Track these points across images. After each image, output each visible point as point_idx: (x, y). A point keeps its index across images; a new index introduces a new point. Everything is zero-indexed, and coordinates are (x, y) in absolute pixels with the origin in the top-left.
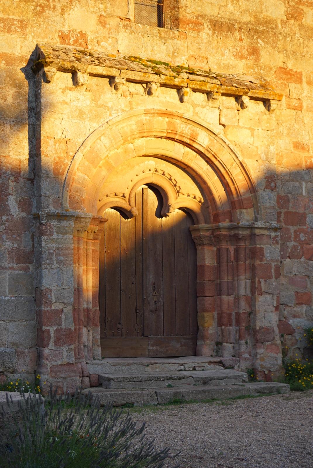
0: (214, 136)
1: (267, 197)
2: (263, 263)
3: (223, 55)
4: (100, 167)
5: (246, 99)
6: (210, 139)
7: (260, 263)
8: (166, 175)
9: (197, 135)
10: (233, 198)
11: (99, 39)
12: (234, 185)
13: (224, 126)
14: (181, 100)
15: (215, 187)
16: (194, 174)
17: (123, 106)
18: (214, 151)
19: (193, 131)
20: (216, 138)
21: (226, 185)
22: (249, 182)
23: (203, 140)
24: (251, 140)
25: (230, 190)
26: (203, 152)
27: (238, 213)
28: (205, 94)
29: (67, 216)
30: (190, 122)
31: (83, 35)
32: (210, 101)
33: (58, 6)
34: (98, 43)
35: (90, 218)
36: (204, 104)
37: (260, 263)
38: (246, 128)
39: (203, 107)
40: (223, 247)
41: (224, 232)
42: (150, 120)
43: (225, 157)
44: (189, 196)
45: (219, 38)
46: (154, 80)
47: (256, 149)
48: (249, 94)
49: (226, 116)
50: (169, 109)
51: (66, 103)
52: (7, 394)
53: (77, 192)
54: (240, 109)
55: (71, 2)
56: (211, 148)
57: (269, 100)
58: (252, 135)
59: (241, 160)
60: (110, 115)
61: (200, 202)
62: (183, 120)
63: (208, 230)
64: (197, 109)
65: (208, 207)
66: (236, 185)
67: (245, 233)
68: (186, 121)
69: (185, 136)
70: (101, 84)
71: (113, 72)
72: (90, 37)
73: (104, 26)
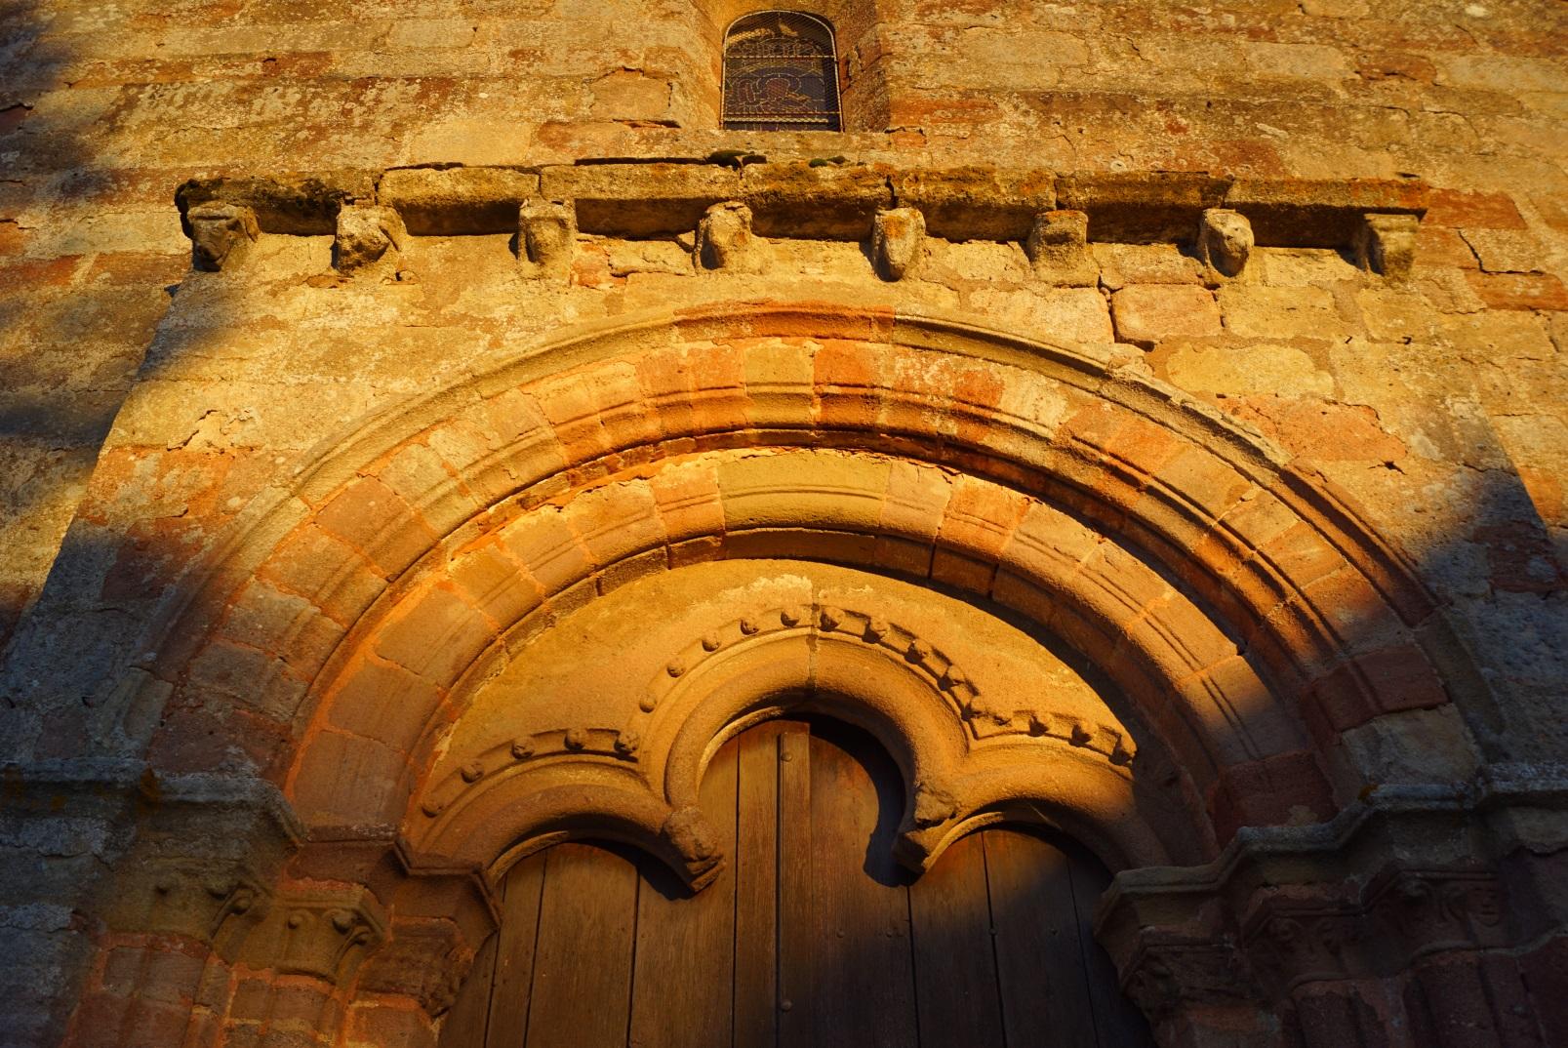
0: (1092, 383)
1: (1529, 635)
6: (1073, 402)
8: (889, 636)
9: (997, 389)
10: (1303, 673)
12: (1280, 593)
13: (1147, 346)
14: (888, 272)
15: (1174, 641)
16: (1042, 607)
18: (1108, 445)
19: (969, 375)
21: (1232, 615)
22: (1370, 565)
23: (1035, 404)
24: (1325, 384)
25: (1237, 594)
26: (1049, 465)
27: (1359, 750)
28: (1015, 245)
29: (66, 787)
30: (941, 341)
32: (1043, 260)
35: (242, 805)
36: (1015, 277)
39: (1012, 288)
40: (1316, 989)
41: (1293, 887)
42: (715, 355)
43: (1183, 463)
44: (1038, 729)
45: (1073, 129)
46: (715, 190)
47: (1363, 417)
48: (1236, 194)
53: (224, 678)
54: (1217, 276)
56: (1092, 436)
59: (1281, 459)
61: (1118, 756)
62: (901, 335)
63: (1188, 899)
65: (1173, 780)
66: (1293, 596)
67: (1442, 855)
68: (918, 339)
69: (927, 400)
70: (472, 255)
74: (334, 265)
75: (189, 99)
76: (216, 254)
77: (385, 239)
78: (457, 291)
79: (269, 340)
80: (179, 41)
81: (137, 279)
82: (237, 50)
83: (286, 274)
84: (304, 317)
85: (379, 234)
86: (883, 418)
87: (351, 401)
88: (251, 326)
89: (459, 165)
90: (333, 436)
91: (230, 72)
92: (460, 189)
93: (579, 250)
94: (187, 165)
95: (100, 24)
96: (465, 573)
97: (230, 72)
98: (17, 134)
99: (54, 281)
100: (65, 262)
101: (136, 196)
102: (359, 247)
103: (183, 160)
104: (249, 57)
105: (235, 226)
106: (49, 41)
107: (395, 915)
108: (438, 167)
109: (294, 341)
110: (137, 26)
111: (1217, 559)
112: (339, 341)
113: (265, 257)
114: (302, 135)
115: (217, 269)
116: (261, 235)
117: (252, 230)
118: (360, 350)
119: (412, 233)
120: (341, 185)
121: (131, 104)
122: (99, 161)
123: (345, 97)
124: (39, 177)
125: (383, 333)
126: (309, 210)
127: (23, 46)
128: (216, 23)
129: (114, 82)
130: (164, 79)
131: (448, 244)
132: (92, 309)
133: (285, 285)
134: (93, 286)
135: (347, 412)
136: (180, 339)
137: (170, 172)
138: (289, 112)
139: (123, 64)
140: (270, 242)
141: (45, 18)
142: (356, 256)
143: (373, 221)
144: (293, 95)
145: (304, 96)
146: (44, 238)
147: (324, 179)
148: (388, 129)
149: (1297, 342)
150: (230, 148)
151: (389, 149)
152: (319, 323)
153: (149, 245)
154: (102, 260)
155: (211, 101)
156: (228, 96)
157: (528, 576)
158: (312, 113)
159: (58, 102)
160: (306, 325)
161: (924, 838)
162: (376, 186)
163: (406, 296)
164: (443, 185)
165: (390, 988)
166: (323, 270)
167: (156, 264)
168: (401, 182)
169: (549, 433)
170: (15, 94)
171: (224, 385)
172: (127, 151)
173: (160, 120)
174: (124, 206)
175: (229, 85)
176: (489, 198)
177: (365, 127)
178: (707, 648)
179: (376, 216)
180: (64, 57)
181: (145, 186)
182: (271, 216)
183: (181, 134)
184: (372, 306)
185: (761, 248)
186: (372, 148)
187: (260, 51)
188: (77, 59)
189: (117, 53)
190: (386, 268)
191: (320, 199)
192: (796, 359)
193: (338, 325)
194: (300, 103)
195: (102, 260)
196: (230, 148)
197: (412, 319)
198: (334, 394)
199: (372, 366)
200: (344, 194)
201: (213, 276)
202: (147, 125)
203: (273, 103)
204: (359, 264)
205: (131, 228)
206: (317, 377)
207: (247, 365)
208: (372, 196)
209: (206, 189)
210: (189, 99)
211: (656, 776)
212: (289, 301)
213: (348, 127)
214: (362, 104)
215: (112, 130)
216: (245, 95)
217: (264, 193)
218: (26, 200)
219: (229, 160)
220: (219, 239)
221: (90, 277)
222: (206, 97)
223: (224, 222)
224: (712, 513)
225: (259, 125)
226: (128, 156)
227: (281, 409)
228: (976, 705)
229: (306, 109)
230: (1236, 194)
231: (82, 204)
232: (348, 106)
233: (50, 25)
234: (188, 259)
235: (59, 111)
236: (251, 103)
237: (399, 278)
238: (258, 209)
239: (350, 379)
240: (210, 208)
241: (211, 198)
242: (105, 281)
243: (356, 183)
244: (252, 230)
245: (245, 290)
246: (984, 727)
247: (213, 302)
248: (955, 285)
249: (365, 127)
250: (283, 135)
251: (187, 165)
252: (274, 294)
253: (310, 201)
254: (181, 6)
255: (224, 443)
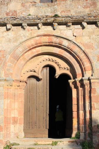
2: (95, 95)
3: (78, 8)
4: (21, 60)
5: (85, 24)
7: (93, 95)
9: (62, 42)
11: (22, 12)
13: (76, 37)
14: (54, 29)
17: (28, 35)
20: (71, 42)
23: (65, 43)
24: (89, 40)
31: (15, 11)
33: (6, 3)
34: (22, 13)
37: (93, 95)
38: (87, 36)
43: (76, 50)
48: (85, 21)
49: (76, 32)
50: (48, 33)
51: (4, 37)
52: (97, 132)
55: (10, 1)
57: (97, 22)
58: (90, 38)
60: (22, 39)
64: (62, 31)
71: (21, 22)
72: (18, 11)
73: (24, 7)
78: (18, 32)
86: (53, 44)
93: (28, 27)
96: (22, 59)
107: (21, 84)
111: (78, 58)
120: (6, 23)
149: (88, 36)
157: (27, 59)
161: (56, 77)
165: (21, 89)
169: (27, 47)
178: (41, 62)
185: (43, 27)
192: (46, 40)
211: (37, 72)
224: (40, 52)
228: (60, 67)
230: (85, 21)
246: (61, 68)
248: (61, 30)
255: (2, 50)
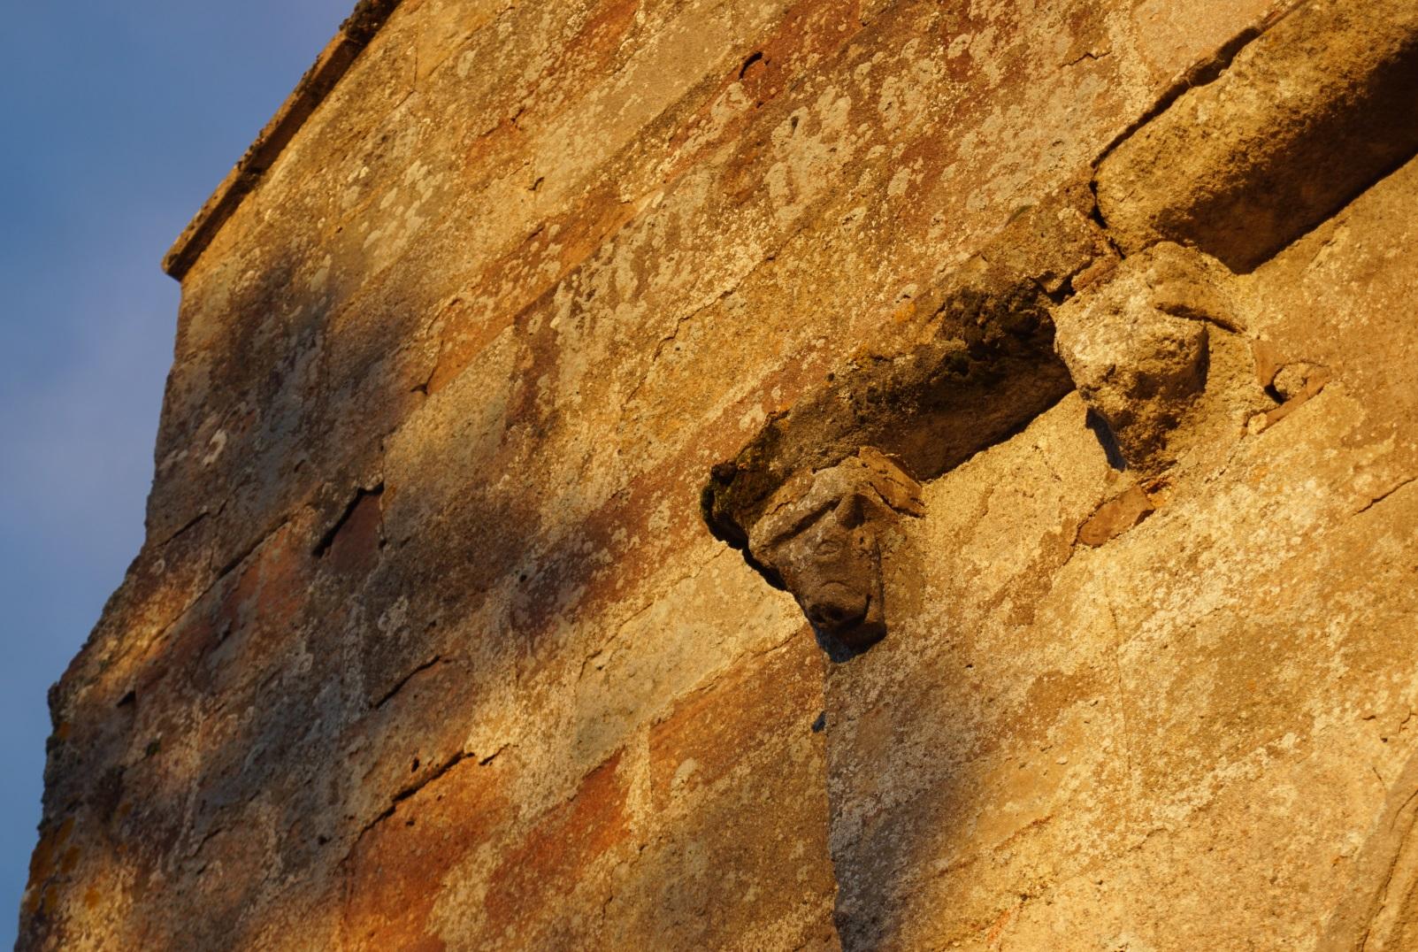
74: (1116, 461)
75: (644, 267)
76: (853, 602)
77: (1189, 328)
79: (1074, 739)
80: (567, 150)
81: (749, 737)
82: (678, 87)
83: (1029, 549)
84: (1121, 635)
85: (1168, 326)
87: (1337, 786)
88: (1017, 726)
89: (1249, 35)
90: (1342, 909)
91: (690, 146)
92: (1286, 90)
94: (713, 414)
95: (415, 222)
97: (690, 146)
98: (384, 557)
99: (598, 843)
100: (599, 783)
101: (653, 550)
102: (1143, 387)
103: (702, 407)
104: (708, 88)
105: (859, 511)
106: (362, 305)
108: (1204, 74)
109: (1130, 708)
110: (477, 175)
112: (1228, 645)
113: (962, 537)
114: (897, 187)
115: (877, 634)
116: (927, 490)
117: (900, 494)
118: (1288, 641)
119: (1244, 265)
120: (1021, 268)
121: (545, 353)
122: (552, 517)
123: (939, 35)
124: (463, 625)
125: (1319, 561)
126: (989, 370)
127: (305, 371)
128: (611, 61)
129: (494, 329)
130: (578, 254)
131: (1343, 236)
132: (697, 864)
133: (1037, 580)
134: (675, 809)
135: (1342, 822)
136: (889, 852)
137: (690, 451)
138: (845, 151)
139: (493, 274)
140: (953, 496)
141: (317, 281)
142: (1151, 409)
143: (1137, 303)
144: (835, 109)
145: (856, 95)
146: (535, 755)
147: (977, 280)
148: (1065, 42)
150: (775, 316)
151: (1094, 85)
152: (1160, 625)
153: (734, 644)
154: (663, 735)
155: (687, 239)
156: (712, 204)
158: (893, 118)
159: (429, 434)
160: (1132, 650)
162: (1097, 216)
163: (1320, 432)
164: (1240, 109)
166: (1100, 489)
167: (769, 680)
168: (1143, 169)
170: (342, 478)
171: (1036, 910)
172: (594, 454)
173: (614, 348)
174: (643, 587)
175: (702, 177)
176: (1366, 64)
177: (1015, 72)
179: (1135, 289)
180: (393, 332)
181: (659, 517)
182: (920, 437)
183: (669, 354)
184: (1262, 503)
186: (1058, 110)
187: (722, 58)
188: (407, 326)
189: (470, 263)
190: (1236, 392)
191: (995, 331)
193: (1203, 605)
194: (856, 115)
195: (663, 735)
196: (775, 316)
197: (1364, 482)
198: (1288, 791)
199: (1338, 666)
200: (1040, 284)
201: (879, 655)
202: (597, 376)
203: (805, 157)
204: (1169, 423)
205: (681, 629)
206: (1228, 771)
207: (1060, 829)
208: (1104, 248)
209: (758, 468)
210: (644, 267)
212: (1066, 614)
213: (981, 98)
214: (979, 24)
215: (541, 435)
216: (742, 178)
217: (873, 396)
218: (465, 698)
219: (787, 346)
220: (842, 564)
221: (659, 790)
222: (673, 236)
223: (830, 518)
225: (804, 225)
226: (597, 471)
227: (1190, 901)
229: (877, 121)
231: (566, 634)
232: (955, 51)
233: (332, 290)
234: (810, 642)
235: (430, 457)
236: (762, 187)
237: (1279, 397)
238: (885, 440)
239: (1304, 729)
240: (788, 504)
241: (776, 483)
242: (691, 784)
243: (1049, 241)
244: (900, 494)
245: (960, 644)
247: (909, 718)
249: (1015, 72)
250: (860, 212)
251: (713, 414)
252: (1026, 616)
253: (977, 349)
254: (531, 74)
